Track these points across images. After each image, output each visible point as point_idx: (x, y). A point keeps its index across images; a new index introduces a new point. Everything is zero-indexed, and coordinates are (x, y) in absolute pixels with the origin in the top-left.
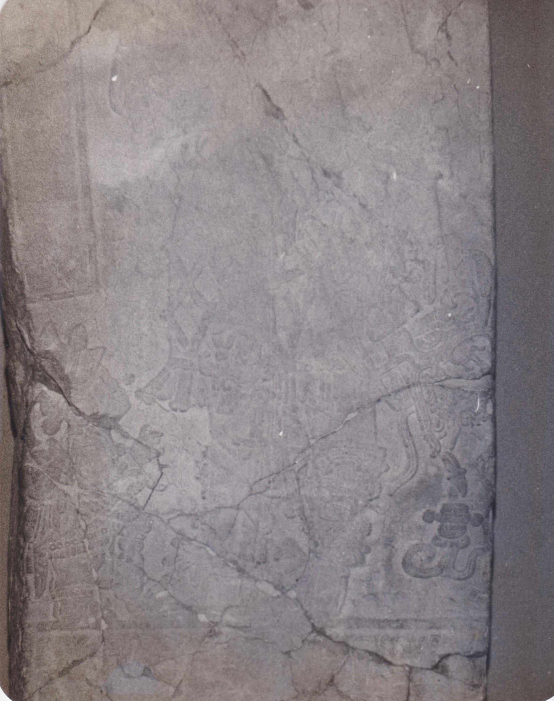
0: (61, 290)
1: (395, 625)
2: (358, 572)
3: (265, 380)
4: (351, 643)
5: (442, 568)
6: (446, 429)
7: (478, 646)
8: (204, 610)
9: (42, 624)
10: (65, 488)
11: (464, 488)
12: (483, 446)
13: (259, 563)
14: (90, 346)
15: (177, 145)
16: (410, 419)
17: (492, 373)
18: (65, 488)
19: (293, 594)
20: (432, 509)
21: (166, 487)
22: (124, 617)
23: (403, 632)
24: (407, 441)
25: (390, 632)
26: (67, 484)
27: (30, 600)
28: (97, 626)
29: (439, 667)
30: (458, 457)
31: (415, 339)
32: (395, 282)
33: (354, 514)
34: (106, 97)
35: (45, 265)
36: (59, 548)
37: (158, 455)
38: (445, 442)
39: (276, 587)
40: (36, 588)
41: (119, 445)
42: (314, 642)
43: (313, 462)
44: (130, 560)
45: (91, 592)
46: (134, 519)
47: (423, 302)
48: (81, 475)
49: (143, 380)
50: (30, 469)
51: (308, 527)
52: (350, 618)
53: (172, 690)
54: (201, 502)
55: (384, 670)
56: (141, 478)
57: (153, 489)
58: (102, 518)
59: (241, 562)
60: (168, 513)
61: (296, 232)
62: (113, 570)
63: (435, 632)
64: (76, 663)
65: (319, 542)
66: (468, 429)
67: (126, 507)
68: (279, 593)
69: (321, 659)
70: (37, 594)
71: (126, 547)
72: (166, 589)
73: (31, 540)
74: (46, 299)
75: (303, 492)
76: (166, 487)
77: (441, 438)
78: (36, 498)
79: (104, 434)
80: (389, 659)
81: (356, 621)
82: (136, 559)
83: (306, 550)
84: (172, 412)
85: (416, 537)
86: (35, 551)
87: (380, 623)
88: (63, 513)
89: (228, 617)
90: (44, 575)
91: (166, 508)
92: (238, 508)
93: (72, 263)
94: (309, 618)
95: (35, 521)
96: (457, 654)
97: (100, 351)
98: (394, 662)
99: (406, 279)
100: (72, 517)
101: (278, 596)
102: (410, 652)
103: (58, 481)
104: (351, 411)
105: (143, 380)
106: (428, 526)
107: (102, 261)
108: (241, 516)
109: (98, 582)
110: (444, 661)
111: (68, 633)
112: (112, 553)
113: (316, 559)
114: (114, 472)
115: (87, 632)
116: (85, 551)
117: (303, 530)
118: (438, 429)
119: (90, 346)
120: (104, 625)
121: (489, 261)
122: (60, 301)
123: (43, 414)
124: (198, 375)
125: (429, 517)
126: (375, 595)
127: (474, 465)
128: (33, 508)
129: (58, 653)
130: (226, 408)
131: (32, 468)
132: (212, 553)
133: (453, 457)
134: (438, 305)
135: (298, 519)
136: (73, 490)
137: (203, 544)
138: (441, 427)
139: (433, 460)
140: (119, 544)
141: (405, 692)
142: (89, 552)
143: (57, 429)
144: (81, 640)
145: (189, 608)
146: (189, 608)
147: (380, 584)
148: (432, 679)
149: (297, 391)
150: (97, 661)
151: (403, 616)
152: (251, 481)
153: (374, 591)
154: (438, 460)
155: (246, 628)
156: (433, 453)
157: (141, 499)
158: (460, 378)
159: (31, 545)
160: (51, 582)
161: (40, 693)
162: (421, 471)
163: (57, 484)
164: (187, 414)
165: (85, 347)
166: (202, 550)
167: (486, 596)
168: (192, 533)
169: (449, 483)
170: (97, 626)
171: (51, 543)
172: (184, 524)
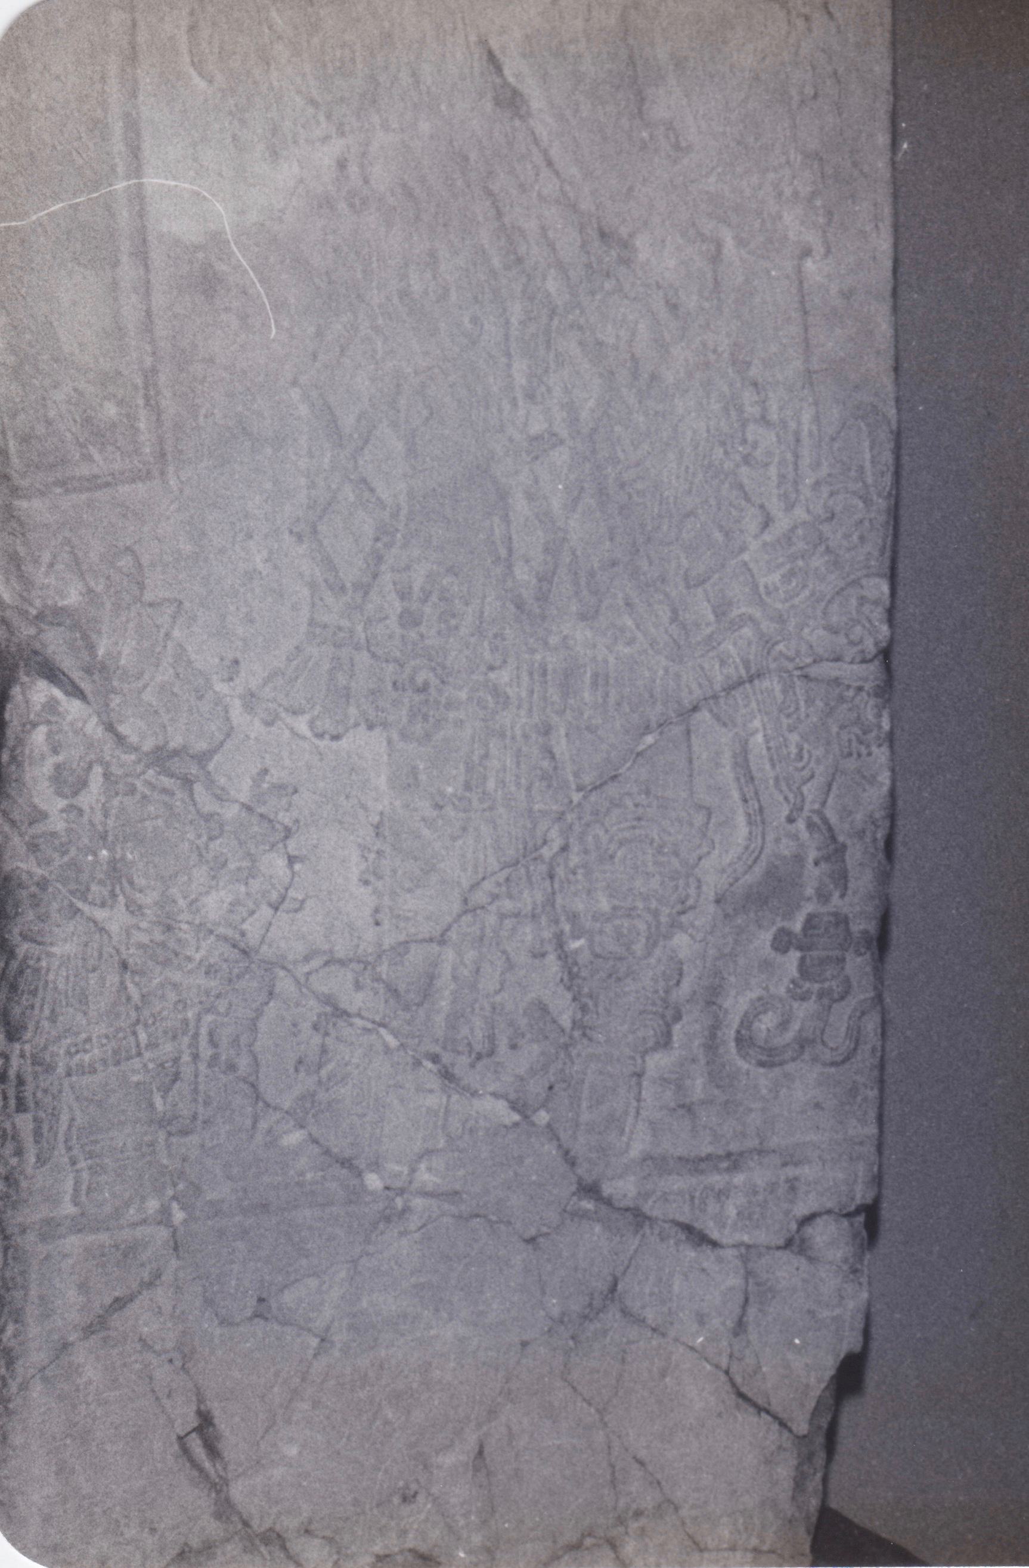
0: (84, 470)
1: (725, 1165)
2: (658, 1062)
3: (491, 668)
4: (647, 1208)
5: (803, 1043)
6: (812, 764)
7: (862, 1195)
8: (376, 1166)
9: (48, 1221)
10: (100, 914)
11: (842, 879)
12: (875, 796)
13: (479, 1057)
14: (148, 596)
15: (326, 156)
16: (752, 741)
17: (886, 654)
18: (100, 914)
19: (543, 1117)
20: (786, 924)
21: (303, 902)
22: (220, 1191)
23: (739, 1179)
24: (746, 789)
25: (717, 1180)
26: (103, 905)
27: (21, 1173)
28: (164, 1216)
29: (795, 1243)
30: (833, 819)
31: (762, 581)
32: (728, 465)
33: (652, 943)
34: (183, 39)
35: (52, 414)
36: (86, 1051)
37: (288, 833)
38: (810, 791)
39: (514, 1106)
40: (37, 1142)
41: (208, 817)
42: (584, 1215)
43: (581, 838)
44: (232, 1067)
45: (151, 1144)
46: (238, 977)
47: (775, 507)
48: (131, 883)
49: (253, 673)
50: (24, 877)
51: (570, 973)
52: (647, 1158)
53: (314, 1342)
54: (370, 934)
55: (708, 1258)
56: (255, 884)
57: (276, 909)
58: (177, 976)
59: (446, 1058)
60: (307, 959)
61: (552, 355)
62: (196, 1091)
63: (790, 1172)
64: (120, 1304)
65: (590, 1003)
66: (851, 764)
67: (226, 949)
68: (516, 1117)
69: (594, 1243)
70: (38, 1157)
71: (224, 1042)
72: (302, 1127)
73: (28, 1035)
74: (58, 490)
75: (559, 901)
76: (303, 902)
77: (804, 783)
78: (39, 939)
79: (179, 795)
80: (715, 1235)
81: (657, 1163)
82: (244, 1063)
83: (565, 1021)
84: (314, 740)
85: (764, 986)
86: (36, 1061)
87: (696, 1164)
88: (94, 970)
89: (425, 1177)
90: (55, 1115)
91: (301, 948)
92: (442, 940)
93: (111, 410)
94: (572, 1163)
95: (34, 993)
96: (829, 1212)
97: (170, 610)
98: (724, 1241)
99: (747, 460)
100: (113, 979)
101: (516, 1125)
102: (750, 1218)
103: (85, 900)
104: (647, 729)
105: (253, 673)
106: (780, 958)
107: (169, 405)
108: (449, 954)
109: (163, 1122)
110: (809, 1230)
111: (103, 1237)
112: (196, 1057)
113: (585, 1041)
114: (200, 874)
115: (140, 1232)
116: (139, 1054)
117: (562, 980)
118: (800, 765)
119: (148, 596)
120: (178, 1216)
121: (889, 423)
122: (84, 497)
123: (55, 751)
124: (363, 658)
125: (783, 942)
126: (689, 1109)
127: (861, 834)
128: (31, 963)
129: (83, 1287)
130: (418, 728)
131: (30, 874)
132: (392, 1042)
133: (825, 821)
134: (800, 513)
135: (552, 958)
136: (116, 919)
137: (374, 1022)
138: (805, 760)
139: (789, 827)
140: (211, 1034)
141: (739, 1298)
142: (147, 1055)
143: (83, 784)
144: (129, 1252)
145: (346, 1163)
146: (346, 1163)
147: (698, 1087)
148: (786, 1271)
149: (551, 690)
150: (162, 1295)
151: (734, 1147)
152: (465, 884)
153: (688, 1101)
154: (801, 825)
155: (454, 1195)
156: (791, 811)
157: (253, 928)
158: (837, 659)
159: (27, 1047)
160: (70, 1127)
161: (45, 1380)
162: (768, 851)
163: (80, 904)
164: (343, 743)
165: (138, 599)
166: (374, 1037)
167: (873, 1094)
168: (355, 1001)
169: (817, 872)
170: (164, 1216)
171: (69, 1041)
172: (338, 984)
